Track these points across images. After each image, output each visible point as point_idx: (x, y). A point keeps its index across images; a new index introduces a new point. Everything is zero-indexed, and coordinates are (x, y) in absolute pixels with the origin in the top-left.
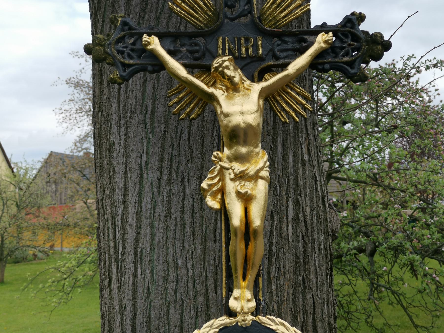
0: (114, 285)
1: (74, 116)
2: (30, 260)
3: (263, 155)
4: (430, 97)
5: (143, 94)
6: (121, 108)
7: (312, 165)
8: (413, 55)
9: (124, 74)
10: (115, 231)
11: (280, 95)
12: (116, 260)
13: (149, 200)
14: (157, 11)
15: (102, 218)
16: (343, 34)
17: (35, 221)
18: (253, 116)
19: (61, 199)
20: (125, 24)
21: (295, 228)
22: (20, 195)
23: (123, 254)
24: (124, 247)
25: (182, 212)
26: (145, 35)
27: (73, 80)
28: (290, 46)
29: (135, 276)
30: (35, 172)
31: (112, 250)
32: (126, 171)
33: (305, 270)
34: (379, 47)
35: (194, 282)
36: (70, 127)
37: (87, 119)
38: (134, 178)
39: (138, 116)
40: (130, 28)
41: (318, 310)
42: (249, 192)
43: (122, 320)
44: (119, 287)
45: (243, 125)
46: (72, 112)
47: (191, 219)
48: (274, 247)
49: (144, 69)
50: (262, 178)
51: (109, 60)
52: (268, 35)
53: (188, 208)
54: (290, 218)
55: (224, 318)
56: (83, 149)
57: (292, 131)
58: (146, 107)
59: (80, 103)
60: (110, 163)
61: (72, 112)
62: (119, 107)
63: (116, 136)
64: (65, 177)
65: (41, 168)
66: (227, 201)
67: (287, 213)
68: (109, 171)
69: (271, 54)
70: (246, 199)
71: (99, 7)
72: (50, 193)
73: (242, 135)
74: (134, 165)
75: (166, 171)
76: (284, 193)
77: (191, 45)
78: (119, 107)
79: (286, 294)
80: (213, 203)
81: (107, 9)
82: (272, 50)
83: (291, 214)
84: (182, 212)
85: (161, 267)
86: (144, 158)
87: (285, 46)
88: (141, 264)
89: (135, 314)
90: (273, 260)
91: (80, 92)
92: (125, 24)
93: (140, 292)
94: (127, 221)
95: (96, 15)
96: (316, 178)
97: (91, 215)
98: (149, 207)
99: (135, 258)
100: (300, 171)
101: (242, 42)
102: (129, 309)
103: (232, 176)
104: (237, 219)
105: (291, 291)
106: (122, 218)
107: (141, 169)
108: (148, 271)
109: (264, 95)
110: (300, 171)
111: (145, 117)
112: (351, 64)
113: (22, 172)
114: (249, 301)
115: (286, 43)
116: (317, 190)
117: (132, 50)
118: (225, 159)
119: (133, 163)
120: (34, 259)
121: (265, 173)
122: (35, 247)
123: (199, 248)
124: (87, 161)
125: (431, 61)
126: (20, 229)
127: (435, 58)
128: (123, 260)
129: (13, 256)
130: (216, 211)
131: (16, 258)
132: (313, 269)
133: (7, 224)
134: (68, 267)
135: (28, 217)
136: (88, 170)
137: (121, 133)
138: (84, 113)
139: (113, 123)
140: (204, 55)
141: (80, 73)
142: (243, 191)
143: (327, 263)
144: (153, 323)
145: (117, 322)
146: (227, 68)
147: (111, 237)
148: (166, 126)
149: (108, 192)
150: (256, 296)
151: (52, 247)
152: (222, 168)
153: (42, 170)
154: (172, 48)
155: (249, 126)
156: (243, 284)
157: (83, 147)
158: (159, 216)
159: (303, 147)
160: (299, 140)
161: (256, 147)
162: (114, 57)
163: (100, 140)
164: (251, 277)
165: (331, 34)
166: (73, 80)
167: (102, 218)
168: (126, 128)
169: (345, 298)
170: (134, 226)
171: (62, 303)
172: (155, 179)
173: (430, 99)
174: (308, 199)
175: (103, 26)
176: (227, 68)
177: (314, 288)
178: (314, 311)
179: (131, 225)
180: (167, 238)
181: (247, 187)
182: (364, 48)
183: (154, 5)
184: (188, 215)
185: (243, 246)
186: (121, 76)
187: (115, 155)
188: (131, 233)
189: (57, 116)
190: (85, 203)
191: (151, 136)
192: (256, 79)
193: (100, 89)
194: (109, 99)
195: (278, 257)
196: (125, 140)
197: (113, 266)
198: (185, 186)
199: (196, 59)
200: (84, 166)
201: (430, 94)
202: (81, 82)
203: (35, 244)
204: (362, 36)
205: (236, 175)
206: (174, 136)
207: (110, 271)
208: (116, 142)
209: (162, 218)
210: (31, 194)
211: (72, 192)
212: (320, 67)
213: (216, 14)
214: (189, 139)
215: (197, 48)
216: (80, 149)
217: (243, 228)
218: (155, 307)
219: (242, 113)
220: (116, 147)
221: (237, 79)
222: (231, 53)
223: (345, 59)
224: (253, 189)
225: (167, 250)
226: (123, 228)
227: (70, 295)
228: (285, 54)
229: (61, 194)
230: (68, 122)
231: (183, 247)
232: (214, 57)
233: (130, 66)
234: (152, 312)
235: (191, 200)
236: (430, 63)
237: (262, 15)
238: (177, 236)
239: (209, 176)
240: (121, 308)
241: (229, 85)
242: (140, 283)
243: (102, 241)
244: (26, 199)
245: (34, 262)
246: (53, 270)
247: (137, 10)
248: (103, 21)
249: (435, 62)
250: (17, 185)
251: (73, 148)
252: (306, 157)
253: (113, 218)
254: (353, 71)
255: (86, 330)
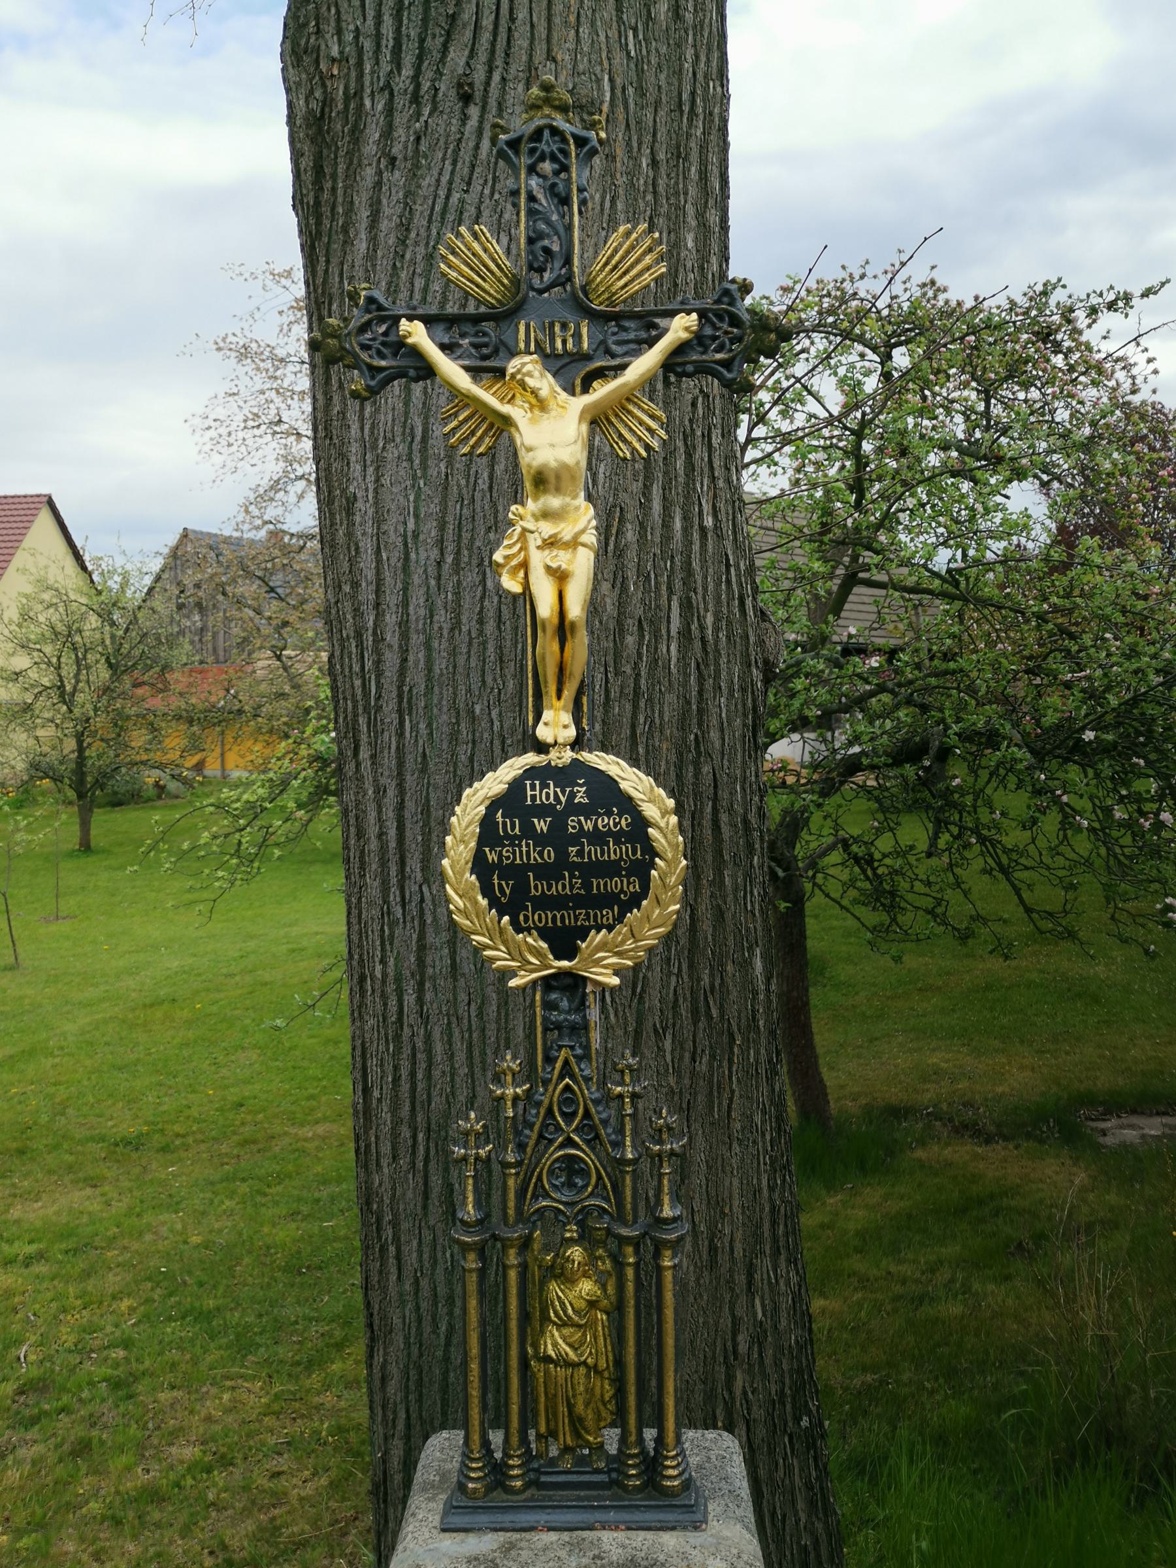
0: (364, 754)
1: (241, 435)
2: (149, 800)
3: (587, 509)
4: (1133, 378)
5: (407, 404)
6: (367, 431)
7: (720, 537)
8: (1059, 280)
9: (373, 383)
10: (363, 657)
11: (617, 415)
12: (366, 710)
13: (422, 601)
14: (427, 244)
15: (336, 636)
16: (716, 315)
17: (157, 703)
18: (569, 450)
19: (215, 649)
20: (371, 300)
21: (683, 650)
22: (113, 637)
23: (378, 698)
24: (379, 686)
25: (481, 622)
26: (403, 321)
27: (234, 339)
28: (632, 336)
29: (401, 734)
30: (148, 581)
31: (359, 692)
32: (379, 548)
33: (700, 725)
34: (773, 336)
35: (503, 743)
36: (230, 465)
37: (274, 444)
38: (393, 561)
39: (397, 446)
40: (380, 308)
41: (724, 794)
42: (564, 566)
43: (380, 812)
44: (373, 757)
45: (553, 464)
46: (234, 425)
47: (497, 633)
48: (643, 681)
49: (401, 374)
50: (584, 545)
51: (349, 360)
52: (595, 317)
53: (491, 614)
54: (674, 632)
55: (530, 754)
56: (266, 523)
57: (681, 472)
58: (412, 429)
59: (253, 403)
60: (349, 535)
61: (234, 425)
62: (362, 429)
63: (359, 483)
64: (224, 594)
65: (163, 571)
66: (532, 579)
67: (669, 622)
68: (349, 549)
69: (602, 348)
70: (560, 576)
71: (319, 233)
72: (188, 635)
73: (552, 480)
74: (394, 538)
75: (450, 547)
76: (664, 588)
77: (476, 335)
78: (362, 429)
79: (663, 763)
80: (511, 584)
81: (334, 237)
82: (603, 342)
83: (676, 623)
84: (481, 622)
85: (445, 717)
86: (411, 525)
87: (624, 336)
88: (410, 714)
89: (403, 801)
90: (642, 704)
91: (252, 373)
92: (371, 300)
93: (410, 764)
94: (383, 640)
95: (313, 247)
96: (728, 560)
97: (293, 687)
98: (422, 612)
99: (400, 702)
100: (696, 547)
101: (557, 328)
102: (391, 793)
103: (539, 542)
104: (546, 607)
105: (673, 758)
106: (375, 633)
107: (406, 544)
108: (422, 726)
109: (589, 417)
110: (696, 547)
111: (410, 448)
112: (727, 364)
113: (114, 583)
114: (565, 727)
115: (626, 329)
116: (729, 582)
117: (383, 344)
118: (529, 517)
119: (392, 533)
120: (159, 797)
121: (591, 538)
122: (161, 766)
123: (511, 684)
124: (277, 552)
125: (1101, 295)
126: (120, 722)
127: (1112, 288)
128: (379, 708)
129: (108, 790)
130: (515, 597)
131: (115, 793)
132: (714, 721)
133: (89, 706)
134: (248, 802)
135: (139, 692)
136: (280, 576)
137: (368, 479)
138: (263, 427)
139: (353, 459)
140: (496, 352)
141: (251, 321)
142: (554, 565)
143: (745, 715)
144: (434, 814)
145: (372, 815)
146: (529, 374)
147: (356, 668)
148: (450, 464)
149: (347, 588)
150: (577, 722)
151: (199, 767)
152: (524, 530)
153: (165, 576)
154: (446, 340)
155: (565, 466)
156: (559, 704)
157: (266, 518)
158: (441, 628)
159: (704, 502)
160: (695, 489)
161: (575, 497)
162: (356, 356)
163: (329, 492)
164: (569, 693)
165: (694, 316)
166: (234, 339)
167: (336, 636)
168: (377, 469)
169: (887, 861)
170: (396, 647)
171: (238, 883)
172: (432, 562)
173: (1134, 384)
174: (710, 599)
175: (326, 271)
176: (529, 374)
177: (716, 756)
178: (716, 794)
179: (390, 646)
180: (455, 667)
181: (561, 559)
182: (749, 338)
183: (423, 232)
184: (490, 627)
185: (556, 647)
186: (368, 386)
187: (358, 519)
188: (391, 659)
189: (198, 434)
190: (279, 658)
191: (422, 483)
192: (578, 389)
193: (325, 393)
194: (342, 413)
195: (650, 700)
196: (376, 491)
197: (361, 720)
198: (484, 574)
199: (484, 358)
200: (269, 565)
201: (1135, 371)
202: (254, 345)
203: (157, 756)
204: (746, 317)
205: (544, 540)
206: (463, 482)
207: (356, 730)
208: (359, 495)
209: (445, 632)
210: (145, 635)
211: (244, 630)
212: (679, 370)
213: (516, 281)
214: (491, 488)
215: (486, 339)
216: (259, 522)
217: (556, 621)
218: (436, 787)
219: (552, 445)
220: (359, 504)
221: (544, 393)
222: (539, 349)
223: (718, 356)
224: (571, 562)
225: (455, 688)
226: (377, 651)
227: (256, 864)
228: (625, 348)
229: (215, 635)
230: (225, 450)
231: (484, 682)
232: (513, 354)
233: (381, 369)
234: (432, 795)
235: (496, 599)
236: (1100, 300)
237: (588, 283)
238: (473, 664)
239: (506, 542)
240: (377, 791)
241: (534, 401)
242: (409, 748)
243: (340, 678)
244: (132, 648)
245: (160, 803)
246: (212, 809)
247: (390, 242)
248: (328, 262)
249: (1111, 297)
250: (105, 615)
251: (240, 518)
252: (709, 522)
253: (359, 635)
254: (729, 376)
255: (293, 951)
